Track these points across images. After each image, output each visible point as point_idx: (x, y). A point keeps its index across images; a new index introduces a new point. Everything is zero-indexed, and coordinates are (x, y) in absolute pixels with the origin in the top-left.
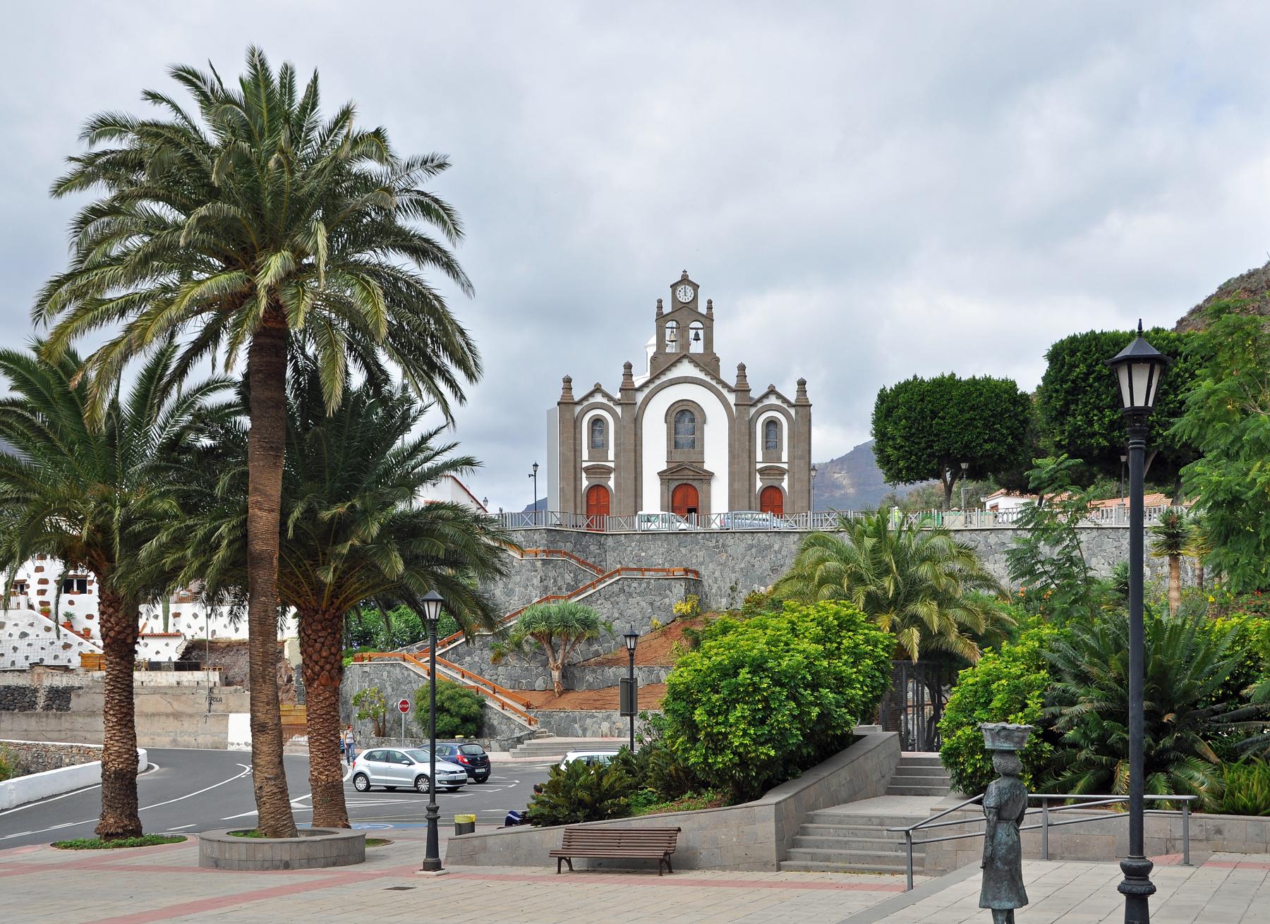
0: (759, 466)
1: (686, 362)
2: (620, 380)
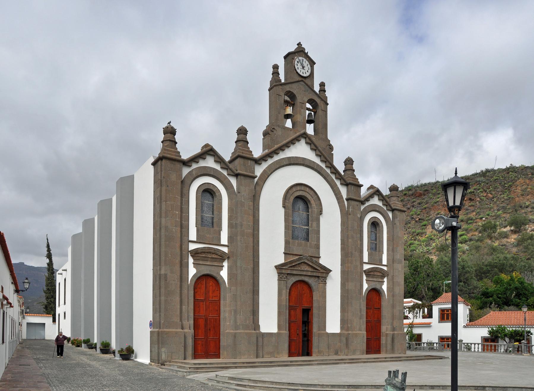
1: (303, 141)
2: (233, 146)
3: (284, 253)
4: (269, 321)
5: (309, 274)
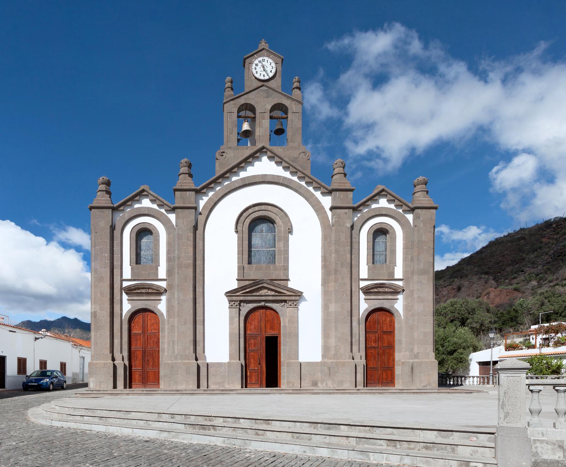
0: (363, 284)
3: (238, 280)
5: (271, 298)
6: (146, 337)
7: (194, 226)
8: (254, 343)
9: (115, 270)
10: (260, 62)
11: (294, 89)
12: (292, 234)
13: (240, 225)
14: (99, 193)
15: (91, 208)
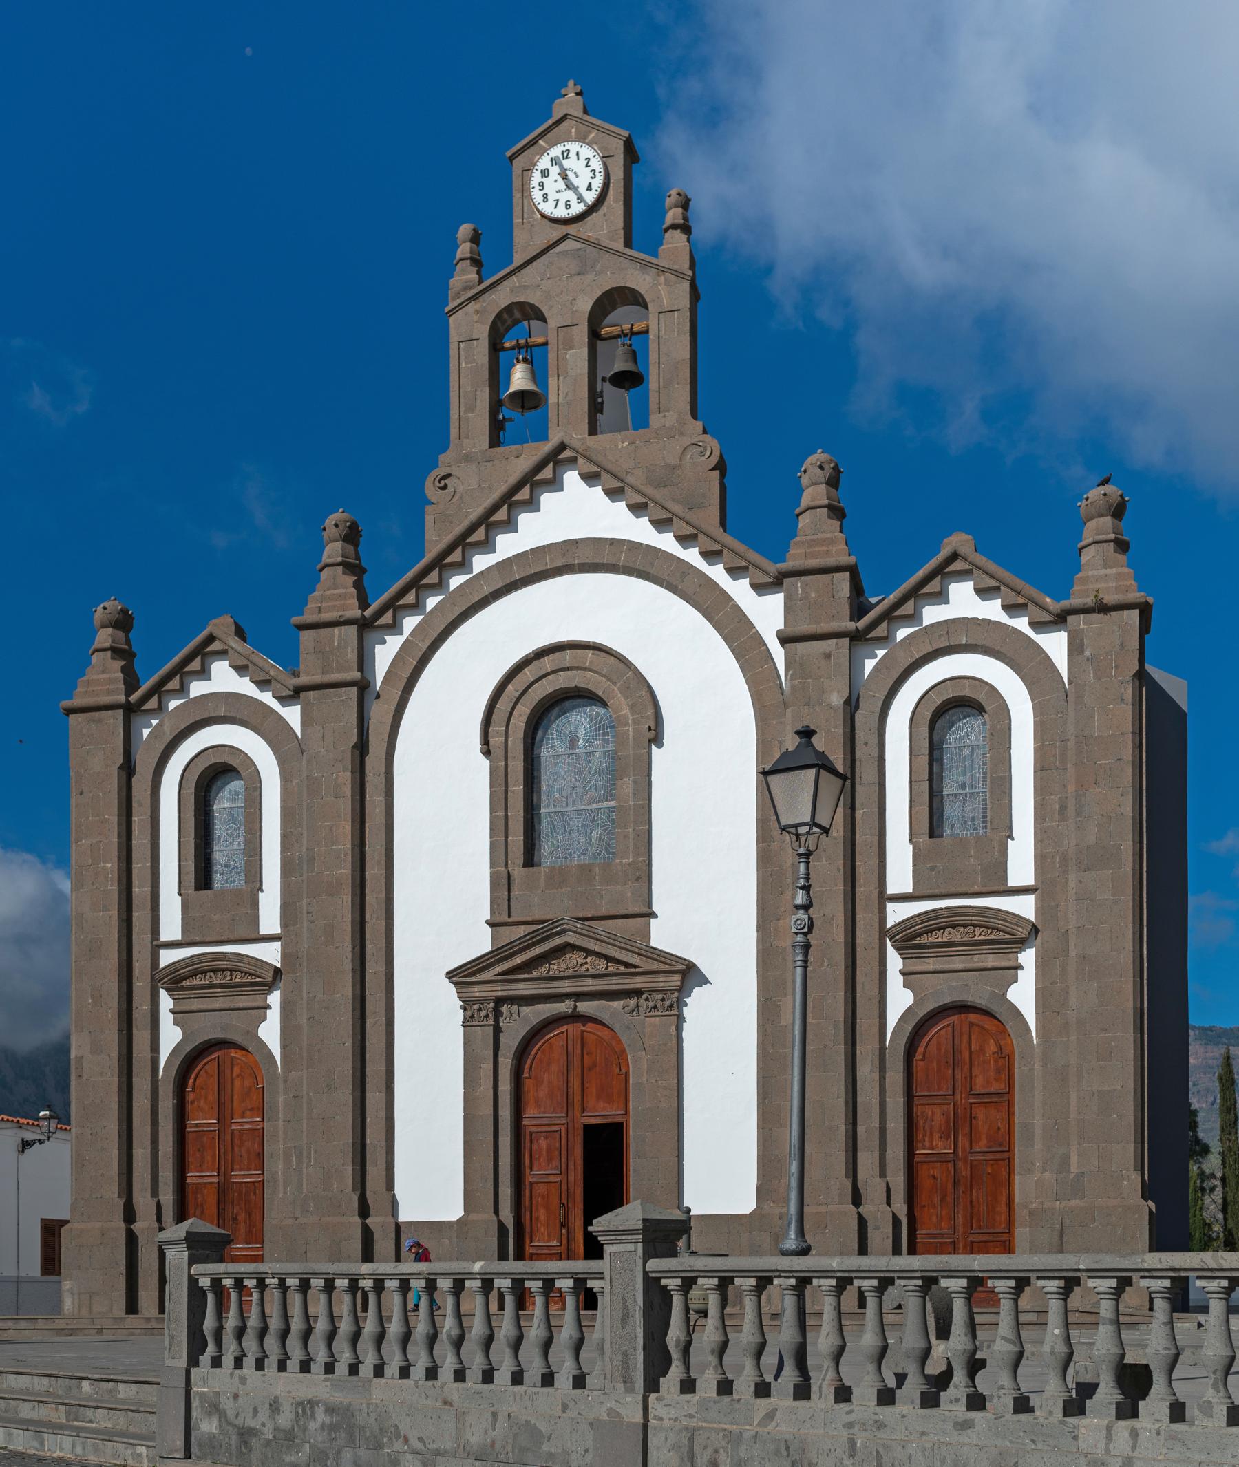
0: (896, 914)
3: (491, 924)
4: (431, 1176)
5: (588, 985)
6: (228, 1138)
7: (121, 768)
8: (549, 1151)
9: (135, 914)
10: (554, 161)
11: (666, 230)
12: (660, 745)
13: (497, 728)
14: (95, 658)
15: (69, 711)
